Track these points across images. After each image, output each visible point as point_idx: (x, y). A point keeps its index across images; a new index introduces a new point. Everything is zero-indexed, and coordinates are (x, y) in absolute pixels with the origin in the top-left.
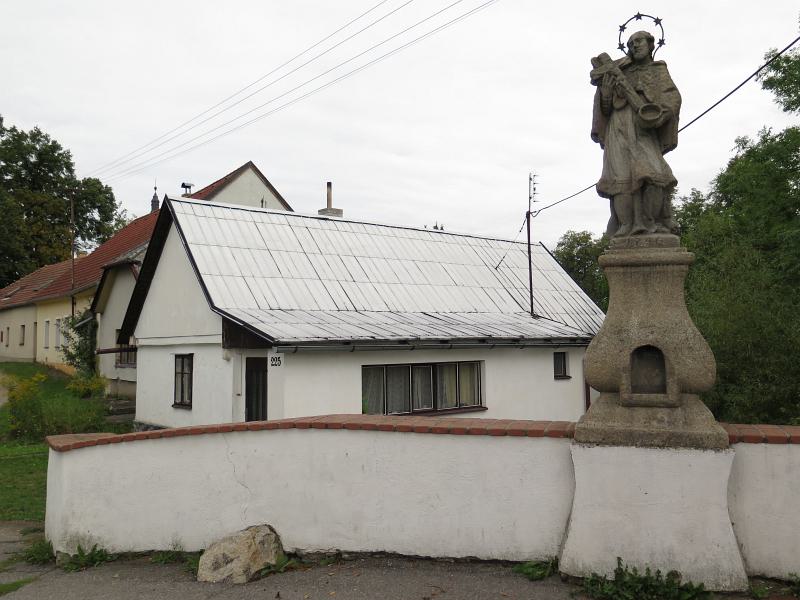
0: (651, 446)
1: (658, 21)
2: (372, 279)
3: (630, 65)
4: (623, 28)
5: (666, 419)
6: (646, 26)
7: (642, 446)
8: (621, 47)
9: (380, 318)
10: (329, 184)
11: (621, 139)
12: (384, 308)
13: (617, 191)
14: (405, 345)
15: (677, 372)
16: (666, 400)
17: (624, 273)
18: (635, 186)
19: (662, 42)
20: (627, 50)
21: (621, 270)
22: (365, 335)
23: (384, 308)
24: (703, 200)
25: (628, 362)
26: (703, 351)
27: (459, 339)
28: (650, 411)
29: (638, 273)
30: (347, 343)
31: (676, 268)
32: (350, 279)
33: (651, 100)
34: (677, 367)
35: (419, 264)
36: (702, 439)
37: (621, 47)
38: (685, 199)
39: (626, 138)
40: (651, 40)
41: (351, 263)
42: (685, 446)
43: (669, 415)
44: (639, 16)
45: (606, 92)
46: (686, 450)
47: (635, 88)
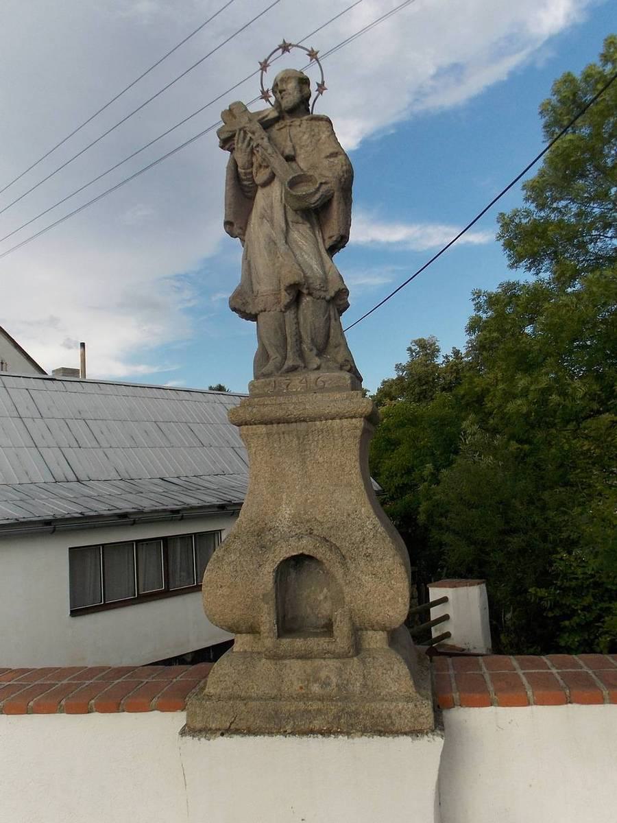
0: (311, 732)
1: (313, 54)
2: (104, 444)
3: (277, 120)
4: (264, 66)
5: (334, 680)
6: (296, 61)
7: (293, 733)
8: (265, 96)
9: (105, 489)
10: (83, 345)
11: (267, 225)
12: (113, 475)
13: (261, 307)
14: (124, 519)
15: (347, 599)
16: (332, 647)
17: (269, 435)
18: (285, 298)
19: (321, 88)
20: (272, 99)
21: (263, 429)
22: (75, 510)
23: (113, 475)
24: (462, 358)
25: (271, 585)
26: (389, 561)
27: (192, 508)
28: (308, 665)
29: (289, 433)
30: (47, 523)
31: (345, 422)
32: (75, 444)
33: (305, 170)
34: (346, 589)
35: (194, 427)
36: (390, 716)
37: (265, 96)
38: (447, 357)
39: (272, 226)
40: (304, 82)
41: (79, 427)
42: (364, 731)
43: (340, 672)
44: (285, 47)
45: (241, 159)
46: (364, 739)
47: (282, 154)
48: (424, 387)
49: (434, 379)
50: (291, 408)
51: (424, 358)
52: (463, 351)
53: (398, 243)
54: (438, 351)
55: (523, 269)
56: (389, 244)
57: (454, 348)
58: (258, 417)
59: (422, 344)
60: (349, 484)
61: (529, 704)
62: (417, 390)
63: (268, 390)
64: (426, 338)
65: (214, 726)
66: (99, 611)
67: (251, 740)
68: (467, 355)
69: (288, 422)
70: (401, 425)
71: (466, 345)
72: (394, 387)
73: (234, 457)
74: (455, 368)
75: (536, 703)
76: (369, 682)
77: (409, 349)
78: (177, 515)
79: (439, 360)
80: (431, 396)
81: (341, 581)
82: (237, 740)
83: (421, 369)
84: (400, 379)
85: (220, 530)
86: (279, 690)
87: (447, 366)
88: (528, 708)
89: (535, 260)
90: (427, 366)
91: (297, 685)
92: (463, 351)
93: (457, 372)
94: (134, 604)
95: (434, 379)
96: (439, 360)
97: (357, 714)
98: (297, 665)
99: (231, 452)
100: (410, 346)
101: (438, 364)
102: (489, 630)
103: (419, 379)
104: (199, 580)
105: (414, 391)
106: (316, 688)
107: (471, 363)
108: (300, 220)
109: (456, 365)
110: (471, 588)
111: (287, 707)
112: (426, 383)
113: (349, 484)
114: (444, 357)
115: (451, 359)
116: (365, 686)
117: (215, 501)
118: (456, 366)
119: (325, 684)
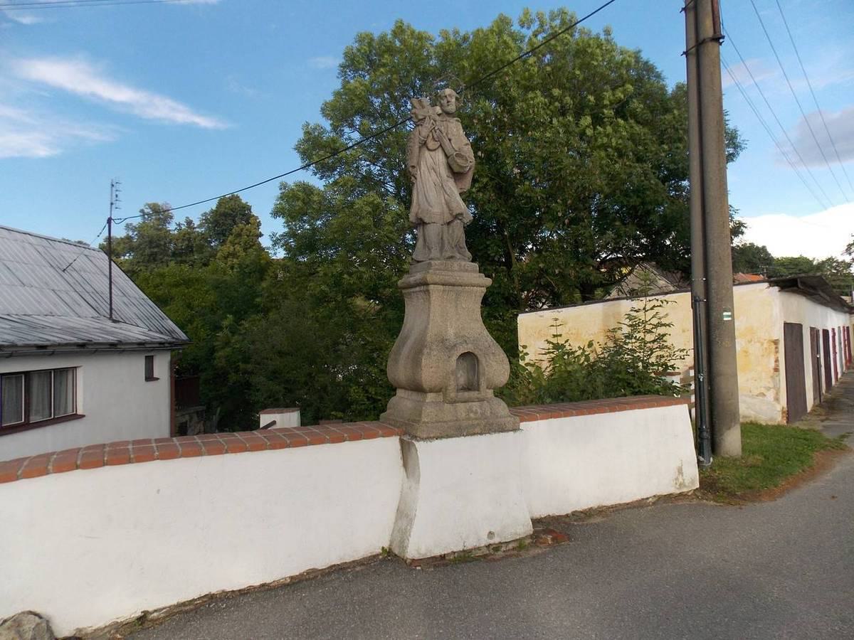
0: (474, 434)
5: (479, 411)
15: (487, 373)
21: (441, 287)
34: (486, 369)
38: (179, 225)
42: (495, 432)
43: (481, 407)
48: (156, 250)
49: (165, 244)
50: (458, 278)
51: (156, 222)
52: (196, 223)
53: (123, 104)
54: (171, 218)
55: (311, 173)
56: (111, 101)
57: (187, 218)
58: (443, 282)
59: (156, 210)
60: (476, 320)
61: (538, 420)
62: (148, 251)
63: (442, 267)
64: (160, 203)
65: (432, 436)
66: (16, 432)
67: (450, 440)
68: (200, 226)
69: (453, 285)
70: (177, 285)
71: (201, 217)
72: (122, 246)
73: (55, 296)
74: (187, 236)
75: (541, 419)
76: (493, 412)
77: (142, 211)
78: (43, 350)
79: (172, 227)
80: (161, 259)
81: (484, 365)
82: (444, 441)
83: (152, 232)
84: (129, 238)
85: (76, 367)
86: (456, 417)
87: (180, 233)
88: (536, 422)
89: (324, 169)
90: (160, 230)
91: (464, 414)
92: (196, 223)
93: (189, 240)
94: (11, 433)
95: (165, 244)
96: (172, 227)
97: (493, 424)
98: (462, 405)
99: (52, 294)
100: (142, 208)
101: (170, 230)
102: (256, 453)
103: (151, 242)
104: (57, 412)
105: (144, 251)
106: (472, 415)
107: (203, 234)
108: (451, 176)
109: (189, 234)
110: (292, 414)
111: (465, 424)
112: (157, 246)
113: (476, 320)
114: (177, 225)
115: (183, 227)
116: (491, 413)
117: (75, 340)
118: (188, 233)
119: (476, 413)
